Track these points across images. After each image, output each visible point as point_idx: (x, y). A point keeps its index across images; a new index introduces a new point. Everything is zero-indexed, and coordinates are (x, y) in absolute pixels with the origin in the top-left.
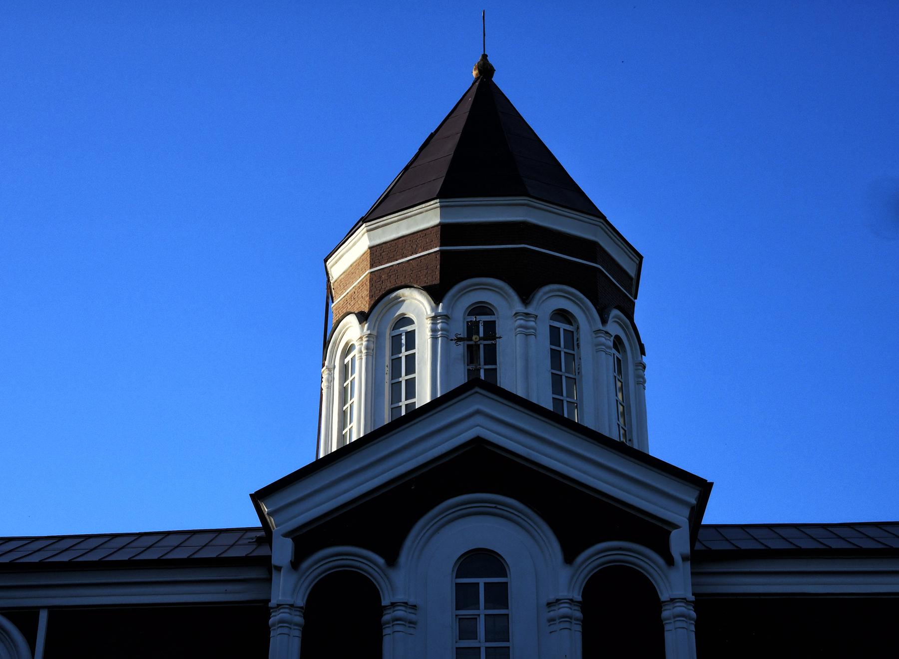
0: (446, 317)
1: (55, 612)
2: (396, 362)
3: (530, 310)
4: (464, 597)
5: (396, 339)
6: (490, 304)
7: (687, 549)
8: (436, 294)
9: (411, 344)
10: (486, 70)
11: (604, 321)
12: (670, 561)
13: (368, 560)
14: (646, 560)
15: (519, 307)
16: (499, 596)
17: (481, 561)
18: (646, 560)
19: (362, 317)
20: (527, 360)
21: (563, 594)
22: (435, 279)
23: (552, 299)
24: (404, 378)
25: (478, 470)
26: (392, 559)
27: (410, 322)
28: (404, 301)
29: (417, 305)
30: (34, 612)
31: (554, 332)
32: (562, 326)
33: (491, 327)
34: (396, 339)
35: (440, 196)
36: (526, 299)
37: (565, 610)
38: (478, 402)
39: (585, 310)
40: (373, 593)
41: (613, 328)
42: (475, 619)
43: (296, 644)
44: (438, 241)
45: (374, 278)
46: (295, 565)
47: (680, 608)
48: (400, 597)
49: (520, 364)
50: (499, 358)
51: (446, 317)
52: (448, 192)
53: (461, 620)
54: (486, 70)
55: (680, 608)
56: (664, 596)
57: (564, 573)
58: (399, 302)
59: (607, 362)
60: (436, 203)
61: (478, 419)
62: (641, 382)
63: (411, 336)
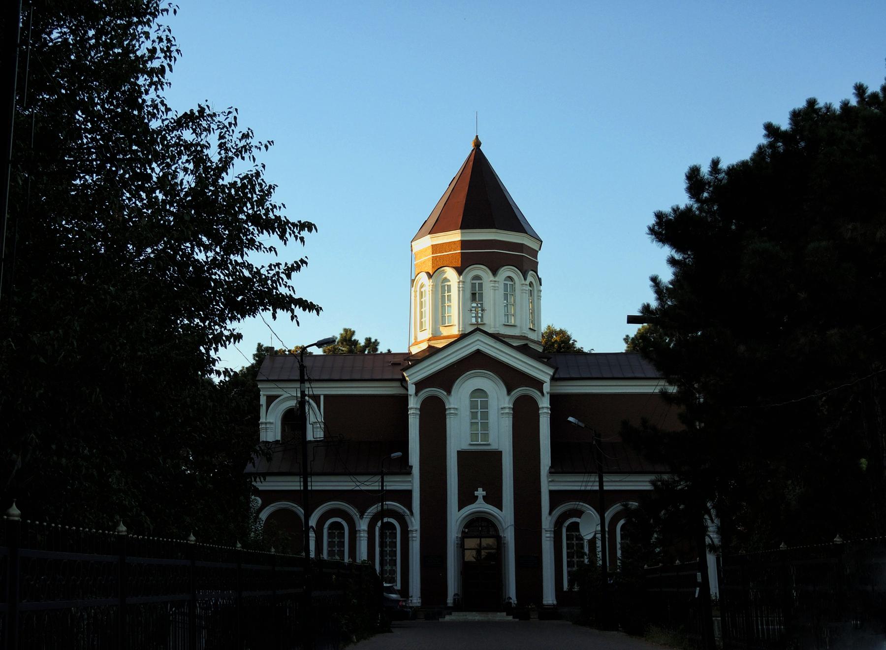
0: (464, 282)
1: (326, 396)
2: (443, 297)
3: (496, 279)
4: (473, 405)
5: (443, 287)
6: (499, 521)
7: (548, 390)
8: (460, 271)
9: (449, 291)
10: (477, 144)
11: (525, 279)
12: (543, 394)
13: (441, 393)
14: (535, 393)
15: (492, 278)
16: (485, 405)
17: (479, 392)
18: (535, 393)
19: (430, 276)
20: (494, 300)
21: (506, 405)
22: (459, 265)
23: (506, 272)
24: (446, 294)
25: (479, 361)
26: (449, 392)
27: (449, 281)
28: (438, 225)
29: (451, 274)
30: (319, 396)
31: (506, 285)
32: (509, 283)
33: (481, 285)
34: (443, 287)
35: (461, 228)
36: (494, 272)
37: (507, 411)
38: (478, 336)
39: (519, 278)
40: (443, 404)
41: (530, 279)
42: (477, 412)
43: (418, 420)
44: (459, 247)
45: (434, 259)
46: (416, 394)
47: (545, 410)
48: (452, 406)
49: (492, 302)
50: (484, 299)
51: (464, 282)
52: (465, 225)
53: (472, 413)
54: (477, 144)
55: (545, 410)
56: (540, 406)
57: (507, 398)
58: (444, 272)
59: (526, 296)
60: (459, 231)
61: (478, 342)
62: (539, 297)
63: (449, 286)
